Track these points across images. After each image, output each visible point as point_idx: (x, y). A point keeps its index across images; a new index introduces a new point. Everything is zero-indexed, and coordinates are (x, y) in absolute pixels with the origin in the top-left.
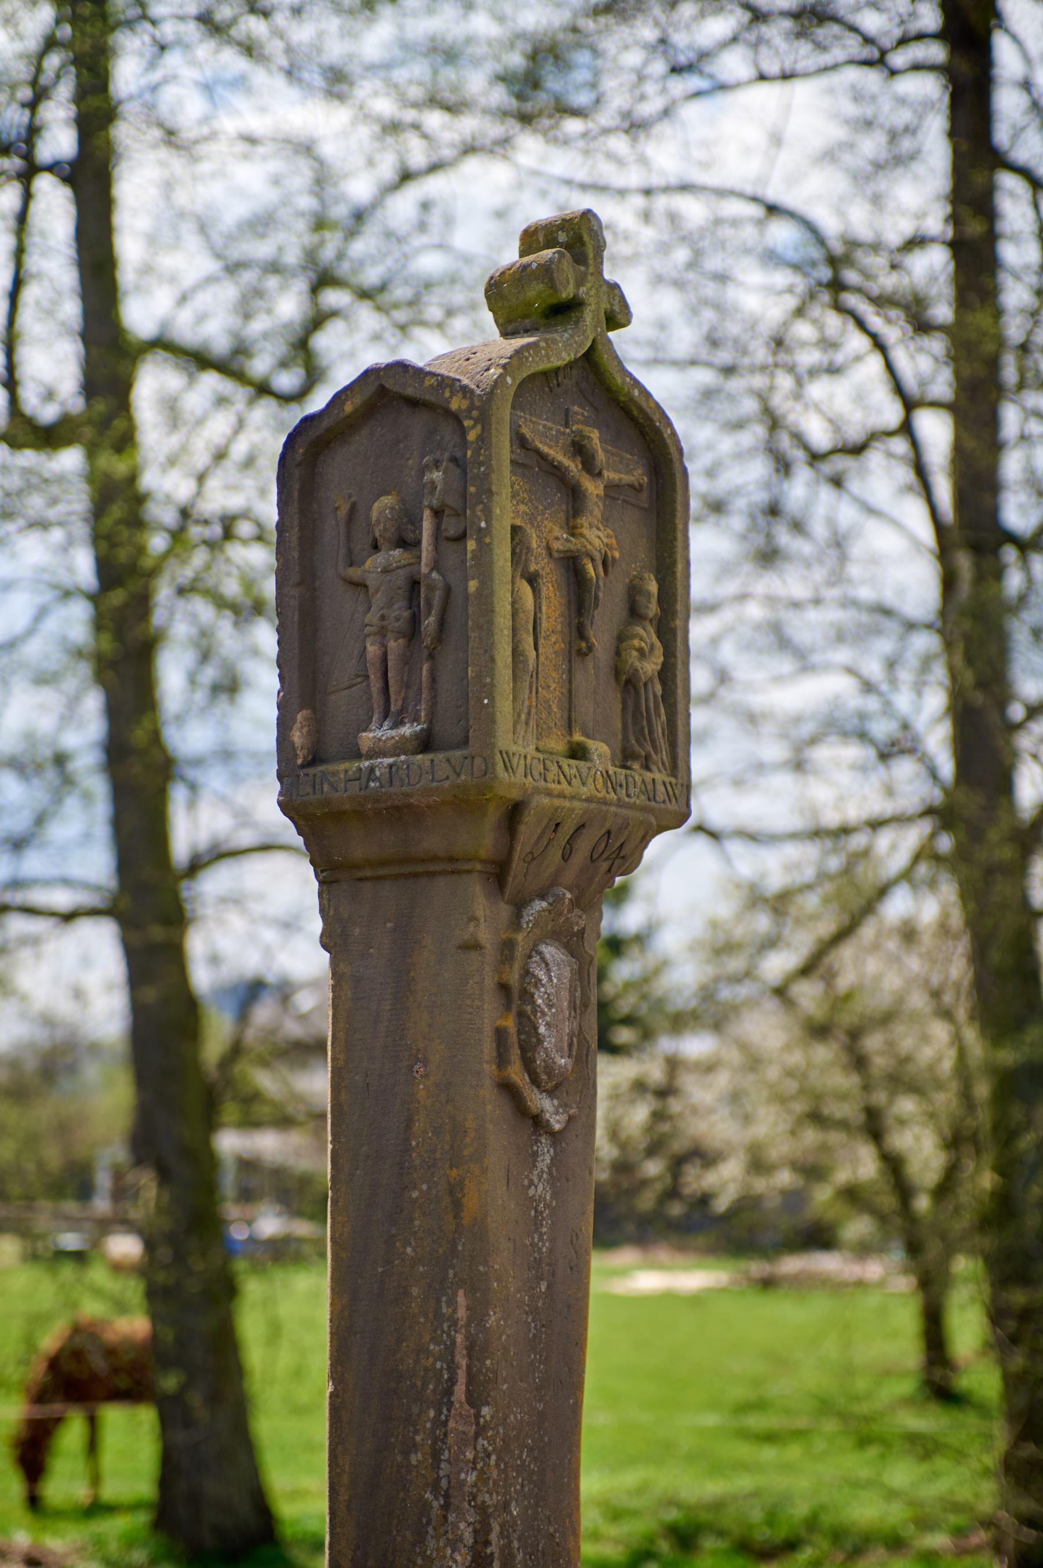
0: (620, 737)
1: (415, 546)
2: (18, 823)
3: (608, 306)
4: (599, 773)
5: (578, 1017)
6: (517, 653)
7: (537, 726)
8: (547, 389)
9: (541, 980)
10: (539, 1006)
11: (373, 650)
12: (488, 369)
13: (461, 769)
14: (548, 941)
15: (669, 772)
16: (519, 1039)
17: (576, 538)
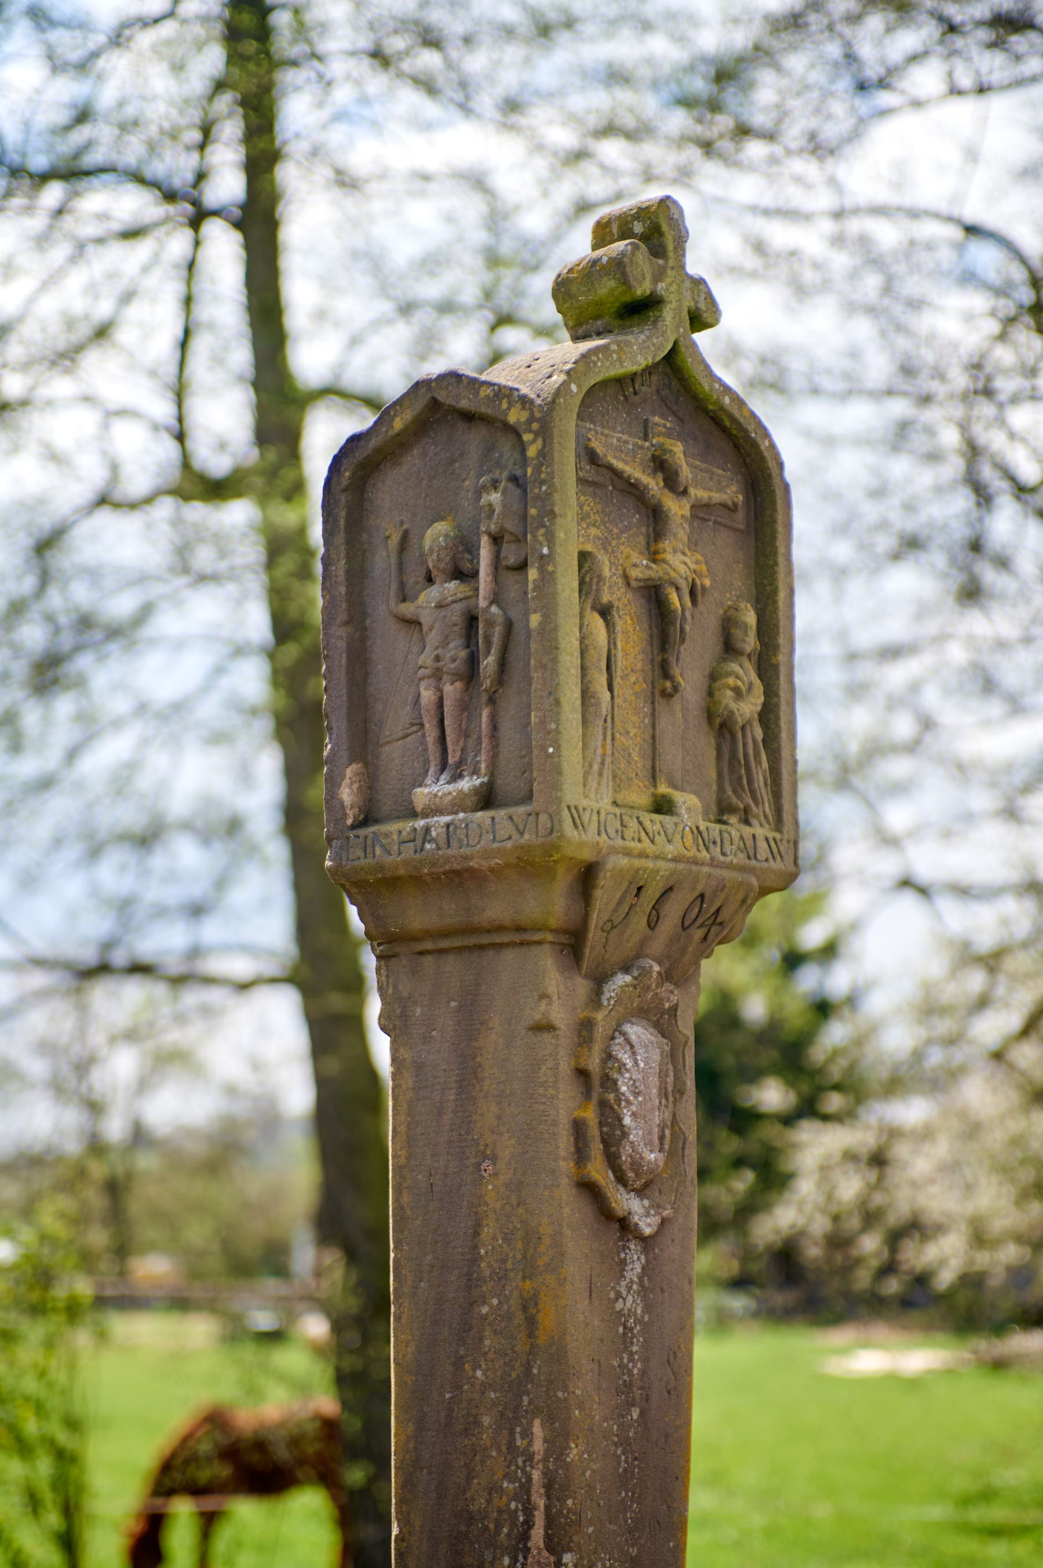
0: (714, 787)
1: (473, 577)
2: (197, 890)
3: (693, 304)
4: (688, 829)
5: (671, 1105)
6: (586, 695)
7: (614, 777)
8: (622, 398)
9: (625, 1065)
10: (623, 1094)
11: (427, 695)
12: (550, 377)
13: (525, 827)
14: (634, 1020)
15: (773, 826)
16: (601, 1132)
17: (658, 565)
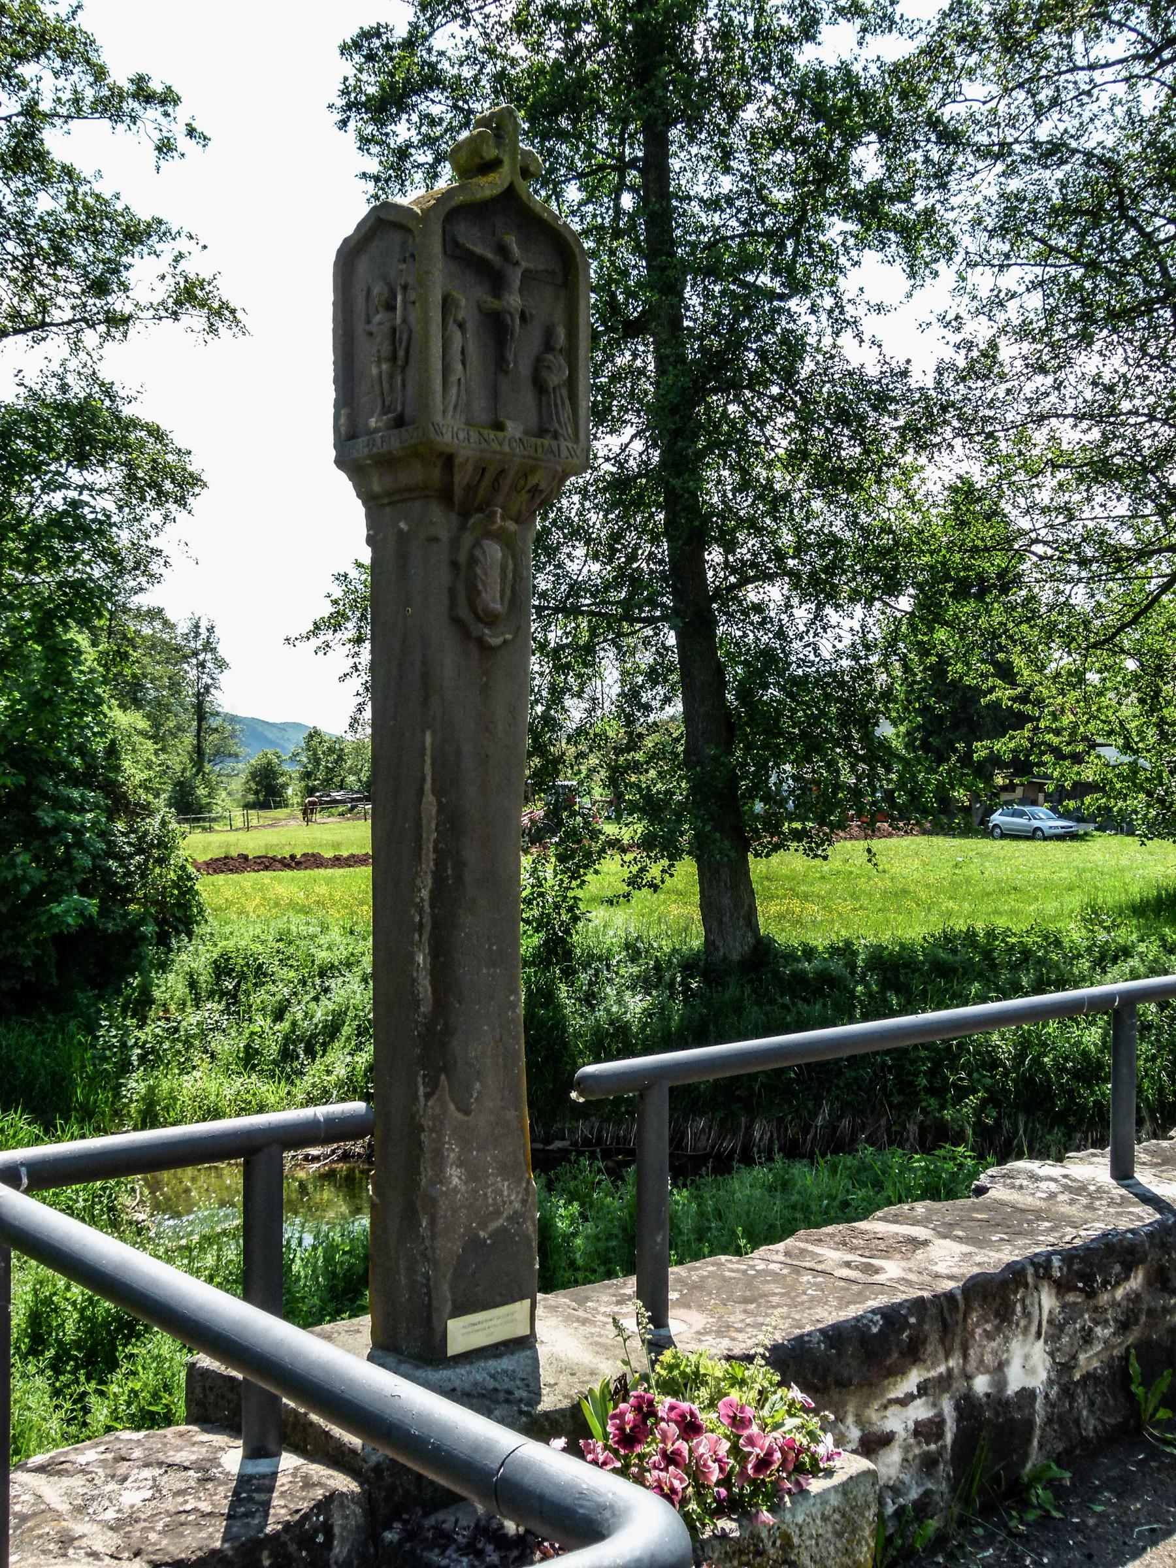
6: (446, 370)
